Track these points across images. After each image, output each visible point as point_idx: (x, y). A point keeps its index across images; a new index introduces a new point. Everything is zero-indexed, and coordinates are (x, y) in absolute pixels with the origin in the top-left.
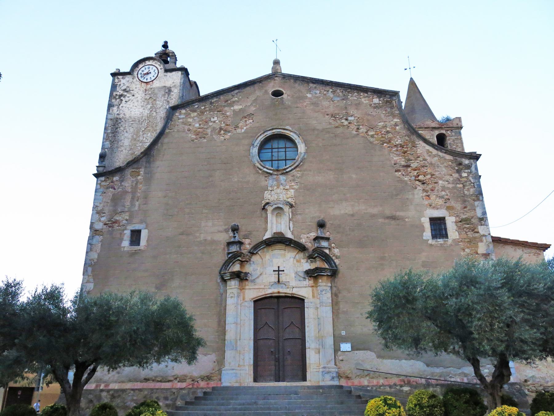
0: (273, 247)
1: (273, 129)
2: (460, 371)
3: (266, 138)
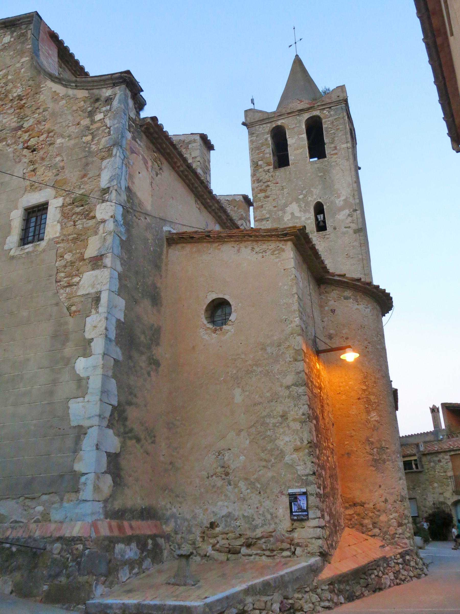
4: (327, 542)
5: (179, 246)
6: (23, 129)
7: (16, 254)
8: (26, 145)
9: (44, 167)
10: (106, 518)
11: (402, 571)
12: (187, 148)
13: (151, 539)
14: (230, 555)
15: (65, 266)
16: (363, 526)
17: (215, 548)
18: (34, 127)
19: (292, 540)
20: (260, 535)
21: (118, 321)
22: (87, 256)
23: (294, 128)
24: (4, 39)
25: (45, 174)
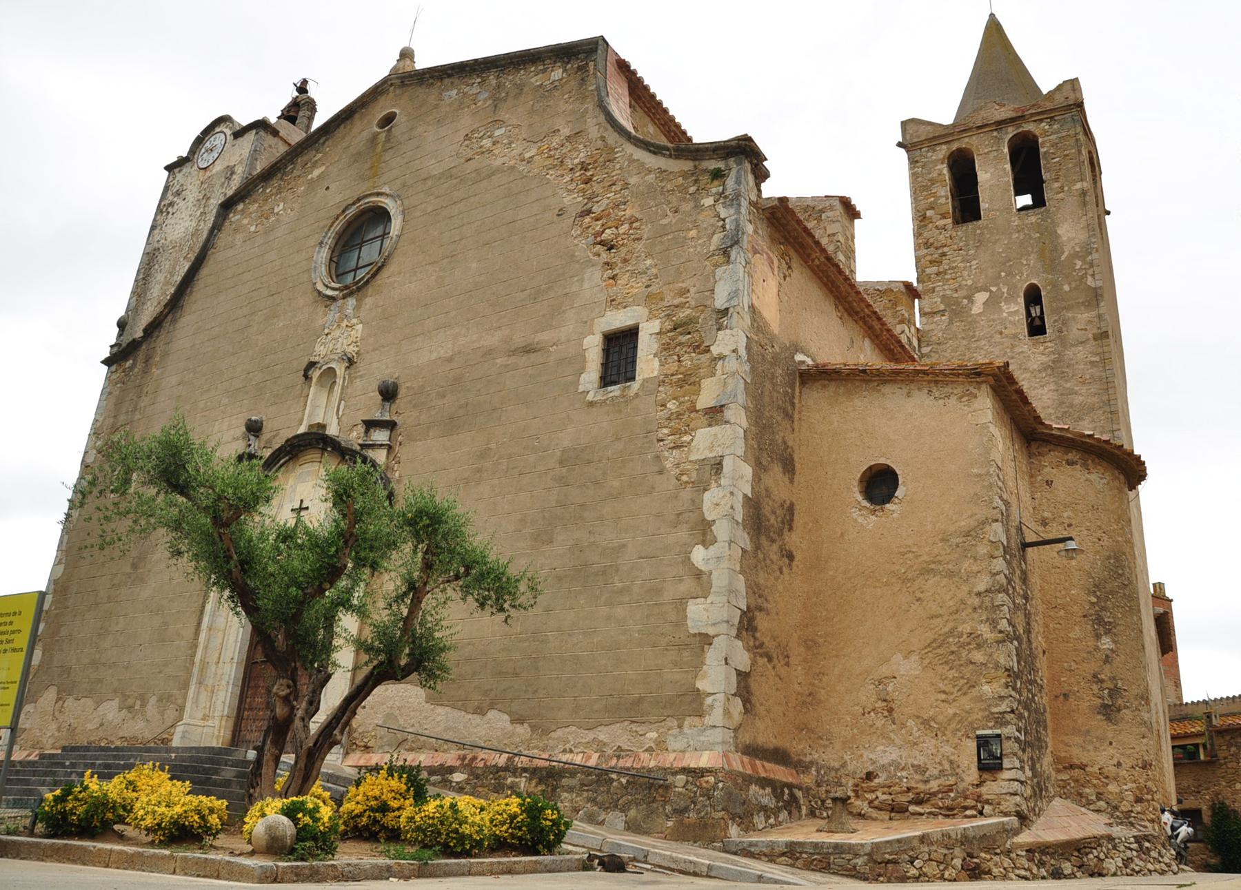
0: (301, 459)
1: (359, 200)
2: (591, 735)
3: (349, 224)
6: (593, 215)
7: (596, 399)
8: (598, 239)
9: (628, 274)
12: (819, 219)
14: (893, 814)
15: (669, 419)
16: (1082, 797)
17: (872, 805)
18: (609, 213)
19: (979, 796)
20: (936, 789)
21: (745, 496)
22: (699, 406)
23: (988, 153)
24: (553, 73)
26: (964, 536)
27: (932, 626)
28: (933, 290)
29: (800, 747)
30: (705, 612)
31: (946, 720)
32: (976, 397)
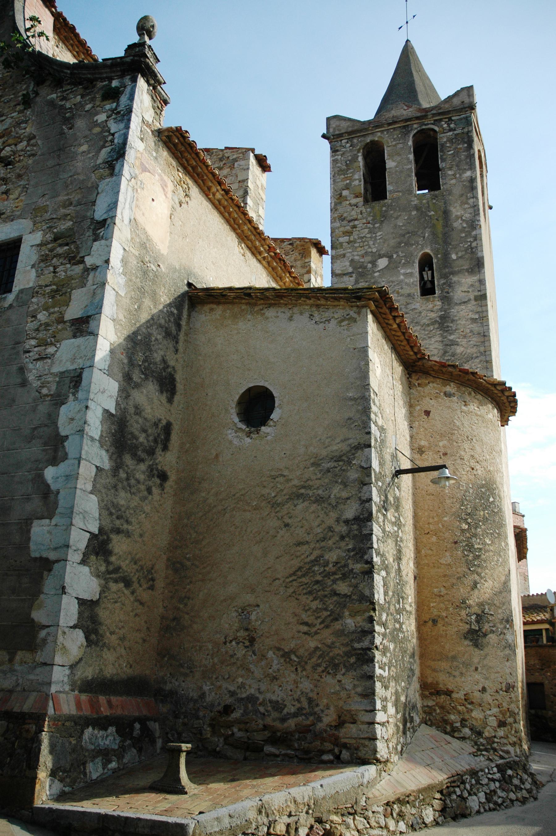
4: (388, 745)
5: (207, 308)
9: (20, 189)
10: (73, 690)
11: (499, 791)
13: (139, 723)
14: (248, 754)
15: (37, 330)
18: (11, 131)
22: (67, 317)
25: (21, 198)
26: (336, 461)
27: (298, 554)
28: (344, 256)
29: (161, 674)
30: (48, 535)
31: (306, 654)
32: (355, 321)
